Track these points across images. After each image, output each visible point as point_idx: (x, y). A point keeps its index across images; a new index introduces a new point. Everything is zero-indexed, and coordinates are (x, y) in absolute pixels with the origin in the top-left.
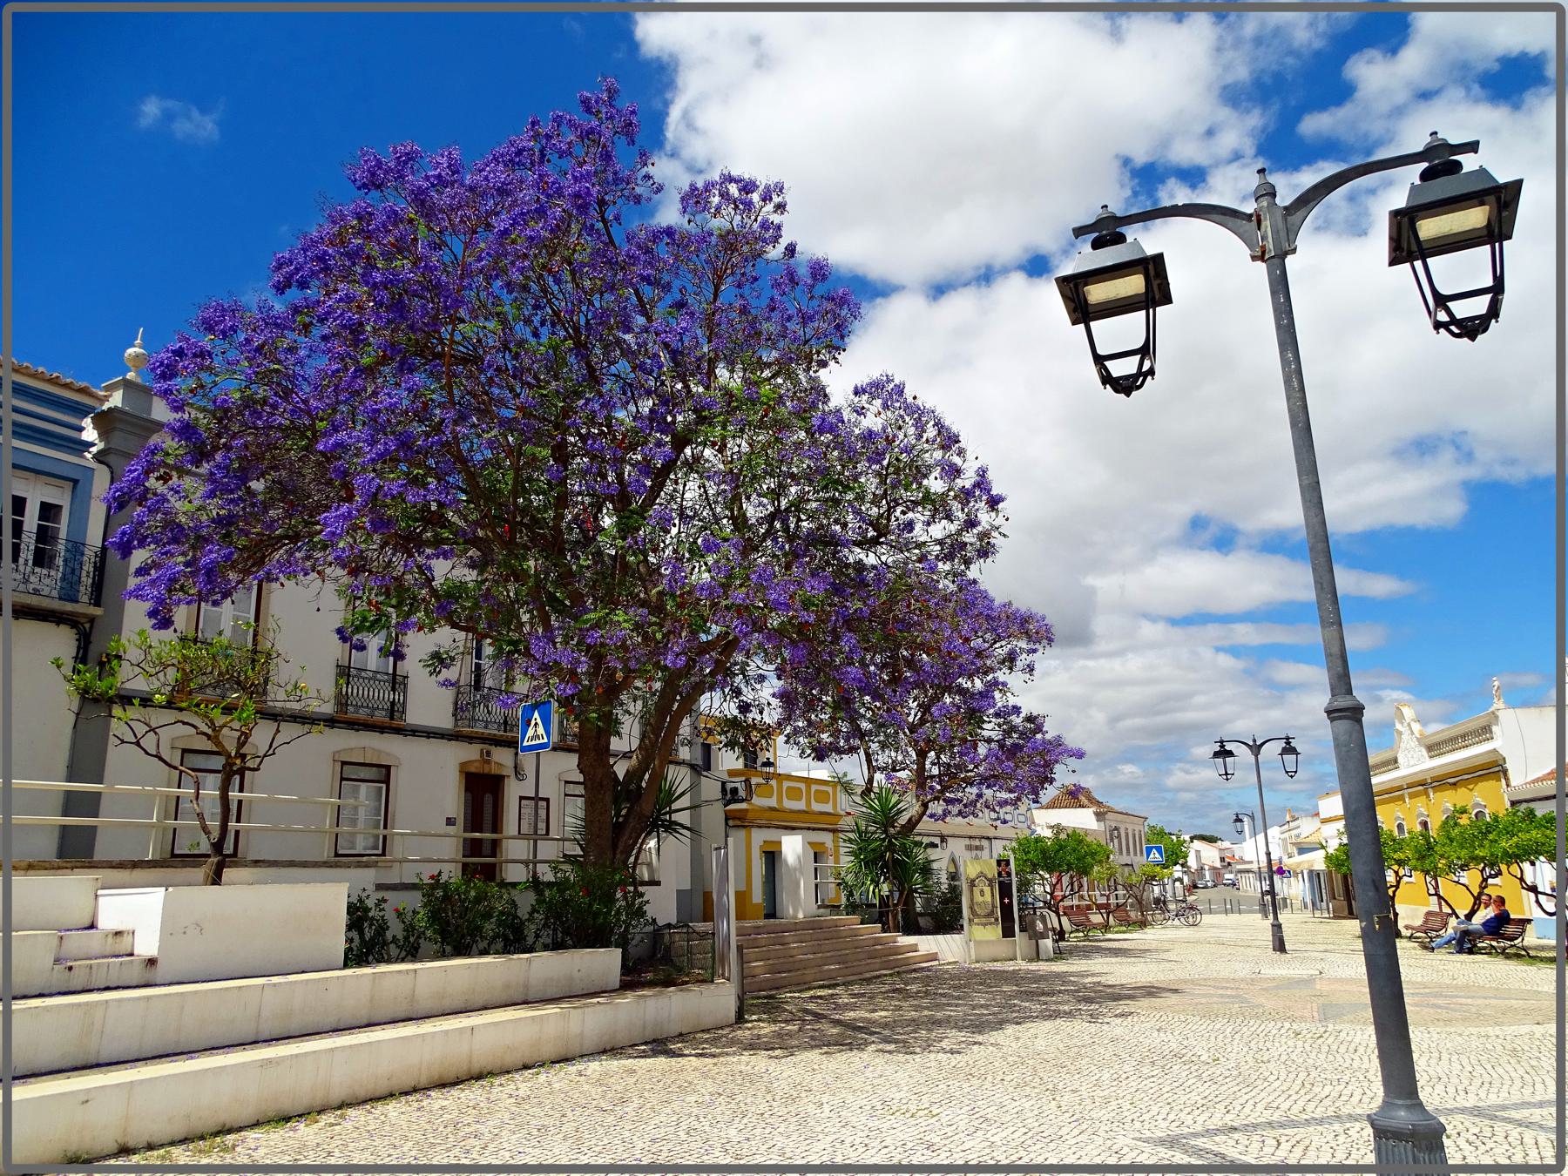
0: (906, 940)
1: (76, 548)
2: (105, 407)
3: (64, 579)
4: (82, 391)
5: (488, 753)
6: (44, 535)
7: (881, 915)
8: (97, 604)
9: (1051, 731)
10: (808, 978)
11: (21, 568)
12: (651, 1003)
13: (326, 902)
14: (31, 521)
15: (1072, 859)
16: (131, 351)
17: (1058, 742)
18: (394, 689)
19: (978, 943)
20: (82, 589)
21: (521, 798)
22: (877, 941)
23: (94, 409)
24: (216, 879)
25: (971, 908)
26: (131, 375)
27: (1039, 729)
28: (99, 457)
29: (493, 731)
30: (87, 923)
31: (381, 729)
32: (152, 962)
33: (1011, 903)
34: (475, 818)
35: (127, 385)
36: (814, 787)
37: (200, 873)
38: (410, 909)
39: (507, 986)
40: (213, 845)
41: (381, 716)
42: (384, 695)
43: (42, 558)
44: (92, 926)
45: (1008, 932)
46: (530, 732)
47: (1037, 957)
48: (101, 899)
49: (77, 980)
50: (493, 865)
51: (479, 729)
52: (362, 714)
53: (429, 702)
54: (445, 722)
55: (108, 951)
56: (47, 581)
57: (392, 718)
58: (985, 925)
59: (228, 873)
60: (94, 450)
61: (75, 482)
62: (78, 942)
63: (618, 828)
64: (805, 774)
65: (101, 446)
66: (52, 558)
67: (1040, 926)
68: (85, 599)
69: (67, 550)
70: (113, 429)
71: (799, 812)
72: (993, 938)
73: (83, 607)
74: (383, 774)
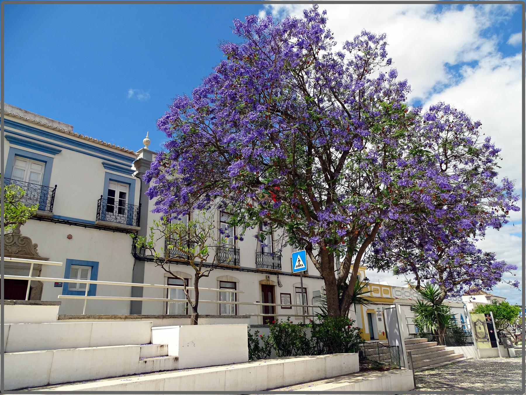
0: (448, 349)
1: (131, 206)
2: (138, 159)
3: (128, 217)
4: (131, 153)
5: (269, 277)
6: (121, 203)
7: (434, 337)
8: (139, 226)
9: (499, 259)
10: (420, 365)
11: (115, 214)
12: (384, 379)
13: (237, 334)
14: (117, 198)
15: (504, 313)
16: (145, 140)
17: (504, 263)
18: (235, 254)
19: (481, 350)
20: (134, 221)
21: (281, 294)
22: (438, 350)
23: (135, 159)
24: (196, 323)
25: (476, 335)
26: (145, 148)
27: (493, 259)
28: (137, 176)
29: (270, 269)
30: (148, 342)
31: (232, 269)
32: (176, 359)
33: (494, 332)
34: (265, 299)
35: (144, 151)
36: (383, 288)
37: (189, 320)
38: (266, 336)
39: (318, 371)
40: (193, 308)
41: (232, 264)
42: (231, 257)
43: (121, 211)
44: (150, 343)
45: (494, 345)
46: (297, 264)
47: (509, 356)
48: (153, 331)
49: (149, 369)
50: (273, 317)
51: (265, 268)
52: (225, 264)
53: (247, 259)
54: (253, 266)
55: (159, 354)
56: (123, 218)
57: (235, 265)
58: (483, 342)
59: (200, 320)
60: (135, 173)
61: (130, 184)
62: (148, 350)
63: (341, 301)
64: (378, 283)
65: (137, 172)
66: (124, 210)
67: (509, 342)
68: (135, 224)
69: (129, 207)
70: (141, 166)
71: (379, 298)
72: (488, 348)
73: (134, 227)
74: (234, 285)
